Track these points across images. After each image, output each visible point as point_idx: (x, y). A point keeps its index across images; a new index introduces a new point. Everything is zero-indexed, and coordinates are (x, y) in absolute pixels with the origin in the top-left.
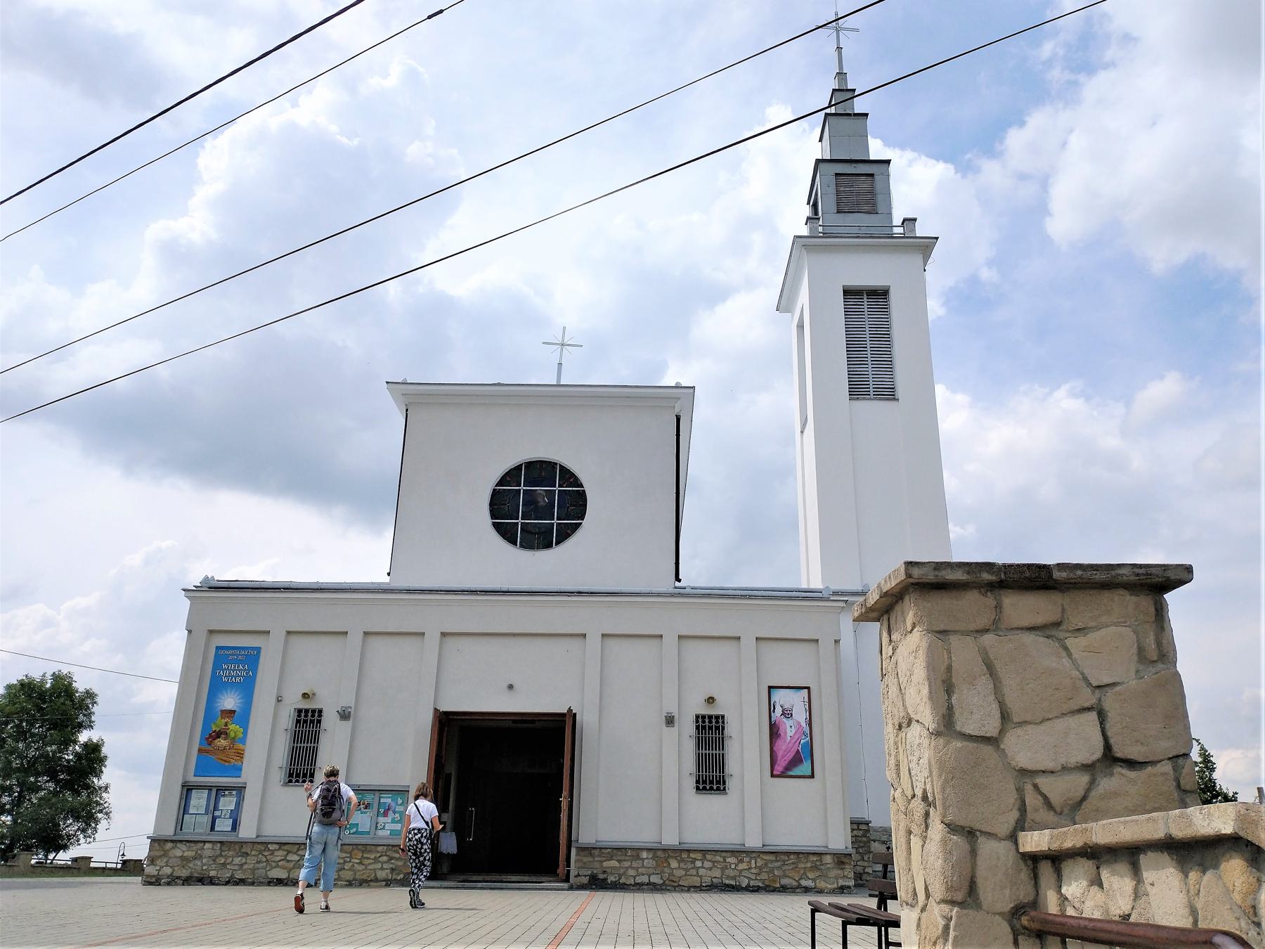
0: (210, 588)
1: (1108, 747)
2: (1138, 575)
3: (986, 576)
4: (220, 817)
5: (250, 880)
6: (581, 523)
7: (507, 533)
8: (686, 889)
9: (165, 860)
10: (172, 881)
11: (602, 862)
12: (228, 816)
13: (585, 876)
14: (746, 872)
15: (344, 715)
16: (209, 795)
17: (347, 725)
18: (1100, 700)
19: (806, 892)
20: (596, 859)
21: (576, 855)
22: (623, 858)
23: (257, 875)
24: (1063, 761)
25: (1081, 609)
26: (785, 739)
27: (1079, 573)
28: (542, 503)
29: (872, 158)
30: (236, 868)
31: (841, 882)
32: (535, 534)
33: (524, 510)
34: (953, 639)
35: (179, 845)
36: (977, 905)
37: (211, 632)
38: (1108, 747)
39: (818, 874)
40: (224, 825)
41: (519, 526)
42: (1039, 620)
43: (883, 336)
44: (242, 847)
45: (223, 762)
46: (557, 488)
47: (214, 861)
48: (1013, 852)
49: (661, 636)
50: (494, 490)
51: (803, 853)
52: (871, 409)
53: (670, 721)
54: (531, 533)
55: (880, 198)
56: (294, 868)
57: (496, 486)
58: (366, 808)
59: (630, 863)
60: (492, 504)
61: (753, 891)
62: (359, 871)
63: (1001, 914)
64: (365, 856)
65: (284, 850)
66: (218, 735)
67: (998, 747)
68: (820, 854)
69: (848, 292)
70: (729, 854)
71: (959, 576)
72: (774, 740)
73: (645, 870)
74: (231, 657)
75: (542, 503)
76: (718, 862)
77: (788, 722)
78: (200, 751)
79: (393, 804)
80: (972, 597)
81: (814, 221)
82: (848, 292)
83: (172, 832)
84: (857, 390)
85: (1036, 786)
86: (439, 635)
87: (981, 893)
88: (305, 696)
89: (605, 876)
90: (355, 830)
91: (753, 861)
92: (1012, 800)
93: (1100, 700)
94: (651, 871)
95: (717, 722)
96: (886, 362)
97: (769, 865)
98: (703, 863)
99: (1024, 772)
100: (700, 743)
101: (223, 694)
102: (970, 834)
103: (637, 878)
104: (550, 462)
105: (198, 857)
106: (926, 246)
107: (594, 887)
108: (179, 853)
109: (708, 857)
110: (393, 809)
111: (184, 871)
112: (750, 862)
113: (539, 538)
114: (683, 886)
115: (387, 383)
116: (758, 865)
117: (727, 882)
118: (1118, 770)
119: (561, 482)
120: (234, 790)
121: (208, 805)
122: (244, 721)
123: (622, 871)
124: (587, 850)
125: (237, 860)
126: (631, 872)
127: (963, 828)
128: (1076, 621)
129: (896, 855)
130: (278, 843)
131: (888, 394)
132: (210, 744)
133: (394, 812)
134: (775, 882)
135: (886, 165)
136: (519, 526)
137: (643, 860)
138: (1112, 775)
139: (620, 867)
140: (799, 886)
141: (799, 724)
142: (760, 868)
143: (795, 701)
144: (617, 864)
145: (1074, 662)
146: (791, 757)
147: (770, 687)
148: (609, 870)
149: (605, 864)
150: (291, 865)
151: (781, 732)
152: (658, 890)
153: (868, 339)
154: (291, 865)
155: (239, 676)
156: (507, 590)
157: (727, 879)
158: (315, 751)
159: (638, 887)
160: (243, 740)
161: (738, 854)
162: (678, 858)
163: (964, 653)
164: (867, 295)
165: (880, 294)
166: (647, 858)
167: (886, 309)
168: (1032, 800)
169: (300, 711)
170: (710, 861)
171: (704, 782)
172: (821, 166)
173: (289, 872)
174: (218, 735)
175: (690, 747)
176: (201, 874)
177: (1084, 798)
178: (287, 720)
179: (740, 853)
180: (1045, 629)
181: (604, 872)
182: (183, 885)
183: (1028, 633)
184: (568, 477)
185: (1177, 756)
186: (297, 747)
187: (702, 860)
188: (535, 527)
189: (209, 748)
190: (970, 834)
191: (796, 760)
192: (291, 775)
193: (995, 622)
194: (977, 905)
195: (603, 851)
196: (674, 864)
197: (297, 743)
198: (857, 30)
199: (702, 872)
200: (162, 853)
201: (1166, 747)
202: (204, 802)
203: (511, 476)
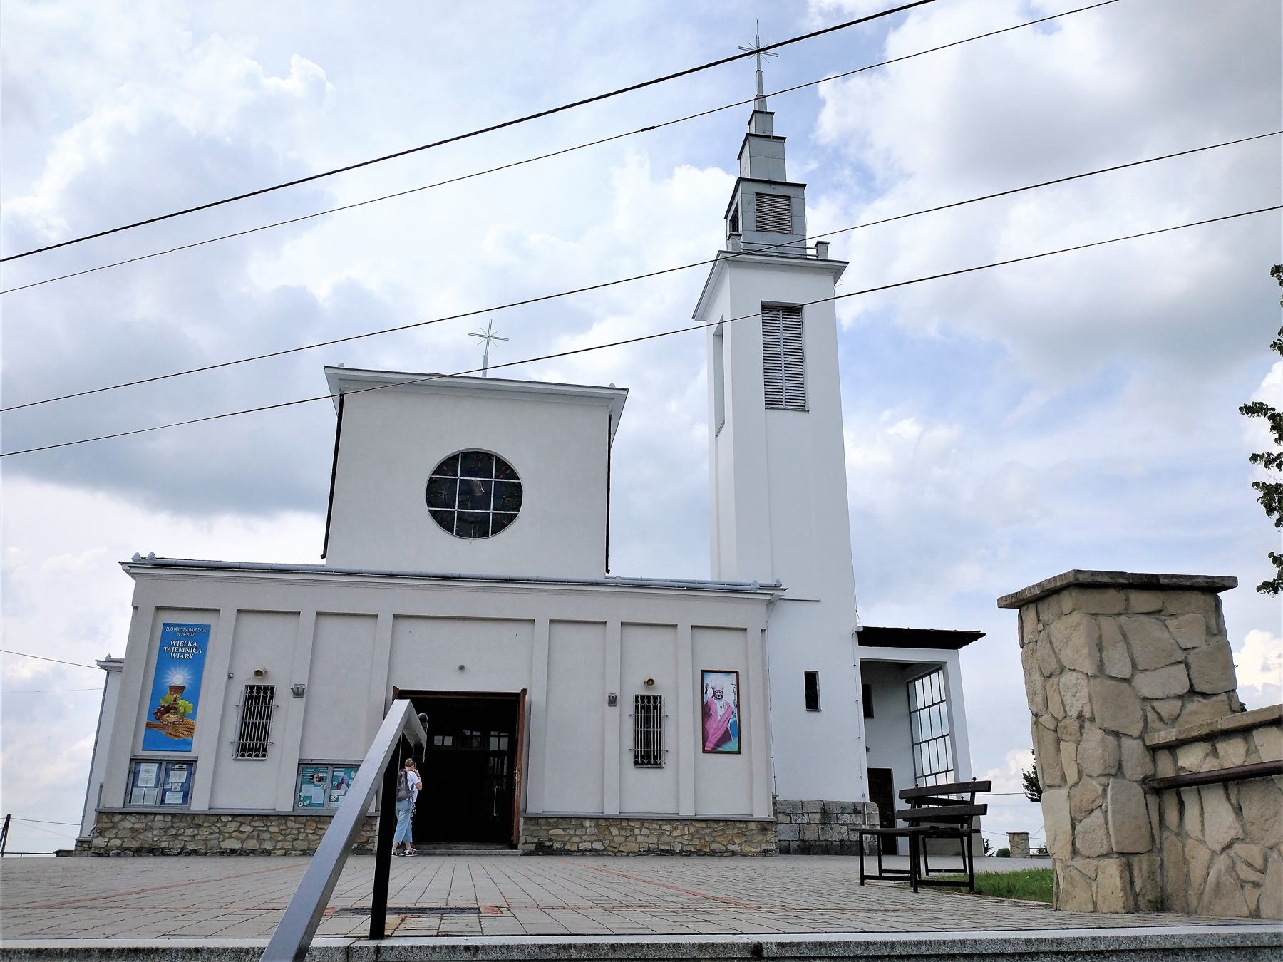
0: (154, 565)
1: (1191, 685)
2: (1208, 582)
3: (1121, 581)
4: (170, 790)
5: (203, 851)
6: (517, 514)
7: (444, 522)
8: (626, 854)
9: (114, 832)
10: (122, 852)
11: (548, 830)
12: (178, 789)
13: (533, 843)
14: (680, 838)
15: (298, 693)
16: (159, 769)
17: (300, 702)
18: (1186, 657)
19: (733, 856)
20: (543, 828)
21: (524, 824)
22: (567, 827)
23: (209, 846)
24: (1167, 692)
25: (1174, 602)
26: (716, 718)
27: (1174, 580)
28: (478, 494)
29: (788, 181)
30: (188, 839)
31: (764, 847)
32: (472, 523)
34: (1100, 618)
35: (128, 817)
36: (1124, 777)
37: (158, 608)
38: (1191, 685)
39: (743, 839)
40: (174, 798)
41: (456, 515)
42: (1151, 609)
43: (797, 351)
44: (193, 819)
45: (173, 737)
46: (493, 479)
47: (164, 832)
48: (1141, 746)
49: (605, 623)
50: (431, 478)
51: (731, 821)
52: (785, 419)
53: (613, 701)
54: (466, 521)
56: (247, 838)
57: (432, 474)
58: (319, 781)
59: (574, 831)
60: (428, 492)
61: (686, 855)
62: (313, 841)
63: (1137, 781)
64: (319, 826)
65: (237, 822)
66: (168, 710)
67: (1130, 685)
68: (746, 822)
70: (665, 823)
71: (1106, 580)
72: (706, 719)
73: (588, 837)
74: (179, 634)
75: (478, 494)
76: (654, 829)
77: (718, 703)
79: (346, 777)
80: (1111, 593)
81: (736, 237)
84: (772, 400)
85: (1153, 708)
86: (392, 616)
87: (1125, 769)
88: (258, 673)
89: (551, 843)
90: (308, 802)
91: (686, 829)
92: (1140, 716)
93: (1186, 657)
94: (594, 838)
95: (655, 702)
96: (799, 376)
97: (701, 832)
98: (641, 831)
99: (1145, 699)
100: (640, 722)
101: (167, 674)
102: (1117, 734)
103: (581, 844)
104: (487, 454)
105: (148, 829)
106: (837, 269)
107: (540, 853)
108: (128, 825)
109: (646, 825)
110: (346, 782)
111: (135, 842)
112: (683, 829)
113: (475, 527)
114: (623, 852)
115: (325, 367)
116: (691, 832)
117: (663, 847)
118: (1197, 698)
119: (497, 474)
120: (185, 764)
122: (194, 697)
123: (567, 838)
124: (534, 820)
125: (189, 832)
126: (576, 840)
127: (1113, 731)
128: (1171, 609)
130: (230, 815)
131: (800, 405)
132: (158, 719)
134: (705, 846)
135: (802, 189)
136: (456, 515)
137: (586, 828)
138: (1193, 702)
139: (565, 835)
140: (727, 851)
141: (728, 704)
142: (693, 835)
143: (724, 684)
144: (562, 833)
145: (1171, 633)
146: (721, 735)
147: (703, 672)
148: (554, 838)
149: (551, 832)
150: (244, 836)
151: (712, 712)
152: (599, 855)
153: (782, 353)
154: (246, 835)
155: (187, 652)
156: (458, 576)
157: (662, 844)
158: (267, 726)
159: (583, 852)
160: (193, 715)
161: (672, 822)
162: (619, 826)
163: (1109, 627)
164: (783, 312)
165: (795, 310)
166: (590, 827)
167: (799, 326)
168: (1151, 716)
169: (252, 688)
170: (647, 828)
171: (643, 757)
172: (743, 184)
173: (242, 842)
174: (168, 710)
175: (630, 726)
176: (151, 845)
177: (1179, 715)
178: (238, 697)
179: (673, 821)
181: (550, 840)
182: (133, 856)
183: (1144, 616)
184: (505, 469)
185: (1229, 691)
186: (249, 723)
187: (642, 827)
188: (472, 516)
190: (1117, 734)
191: (726, 738)
192: (244, 750)
193: (1126, 609)
194: (1124, 777)
195: (549, 820)
196: (615, 832)
197: (250, 718)
199: (640, 838)
200: (111, 825)
201: (1223, 685)
202: (154, 776)
203: (448, 465)
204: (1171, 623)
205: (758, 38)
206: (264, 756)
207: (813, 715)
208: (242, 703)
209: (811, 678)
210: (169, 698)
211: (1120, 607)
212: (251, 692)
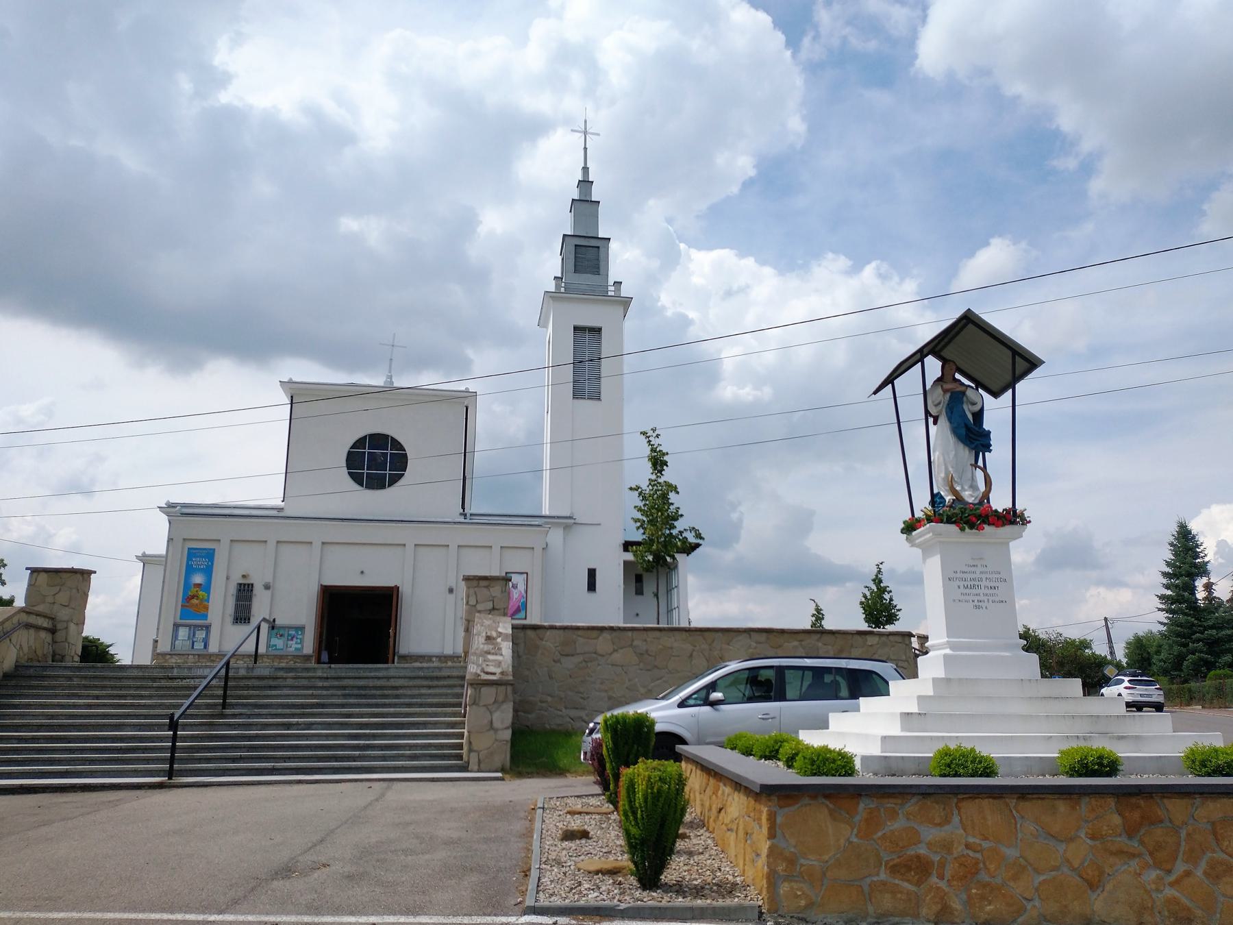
0: (182, 514)
7: (357, 479)
15: (267, 587)
17: (269, 593)
28: (380, 461)
29: (599, 237)
35: (174, 656)
40: (199, 646)
50: (349, 451)
55: (602, 264)
60: (347, 460)
66: (193, 597)
69: (576, 329)
78: (182, 606)
82: (576, 329)
83: (169, 650)
84: (578, 394)
88: (244, 576)
121: (189, 634)
133: (297, 638)
141: (521, 592)
158: (250, 605)
163: (472, 591)
169: (240, 584)
172: (566, 238)
174: (193, 597)
178: (233, 590)
180: (487, 587)
184: (397, 444)
189: (187, 604)
192: (237, 619)
198: (598, 135)
203: (360, 443)
204: (491, 589)
205: (586, 122)
206: (249, 622)
207: (592, 595)
208: (235, 592)
209: (592, 573)
210: (193, 591)
211: (476, 585)
212: (240, 587)
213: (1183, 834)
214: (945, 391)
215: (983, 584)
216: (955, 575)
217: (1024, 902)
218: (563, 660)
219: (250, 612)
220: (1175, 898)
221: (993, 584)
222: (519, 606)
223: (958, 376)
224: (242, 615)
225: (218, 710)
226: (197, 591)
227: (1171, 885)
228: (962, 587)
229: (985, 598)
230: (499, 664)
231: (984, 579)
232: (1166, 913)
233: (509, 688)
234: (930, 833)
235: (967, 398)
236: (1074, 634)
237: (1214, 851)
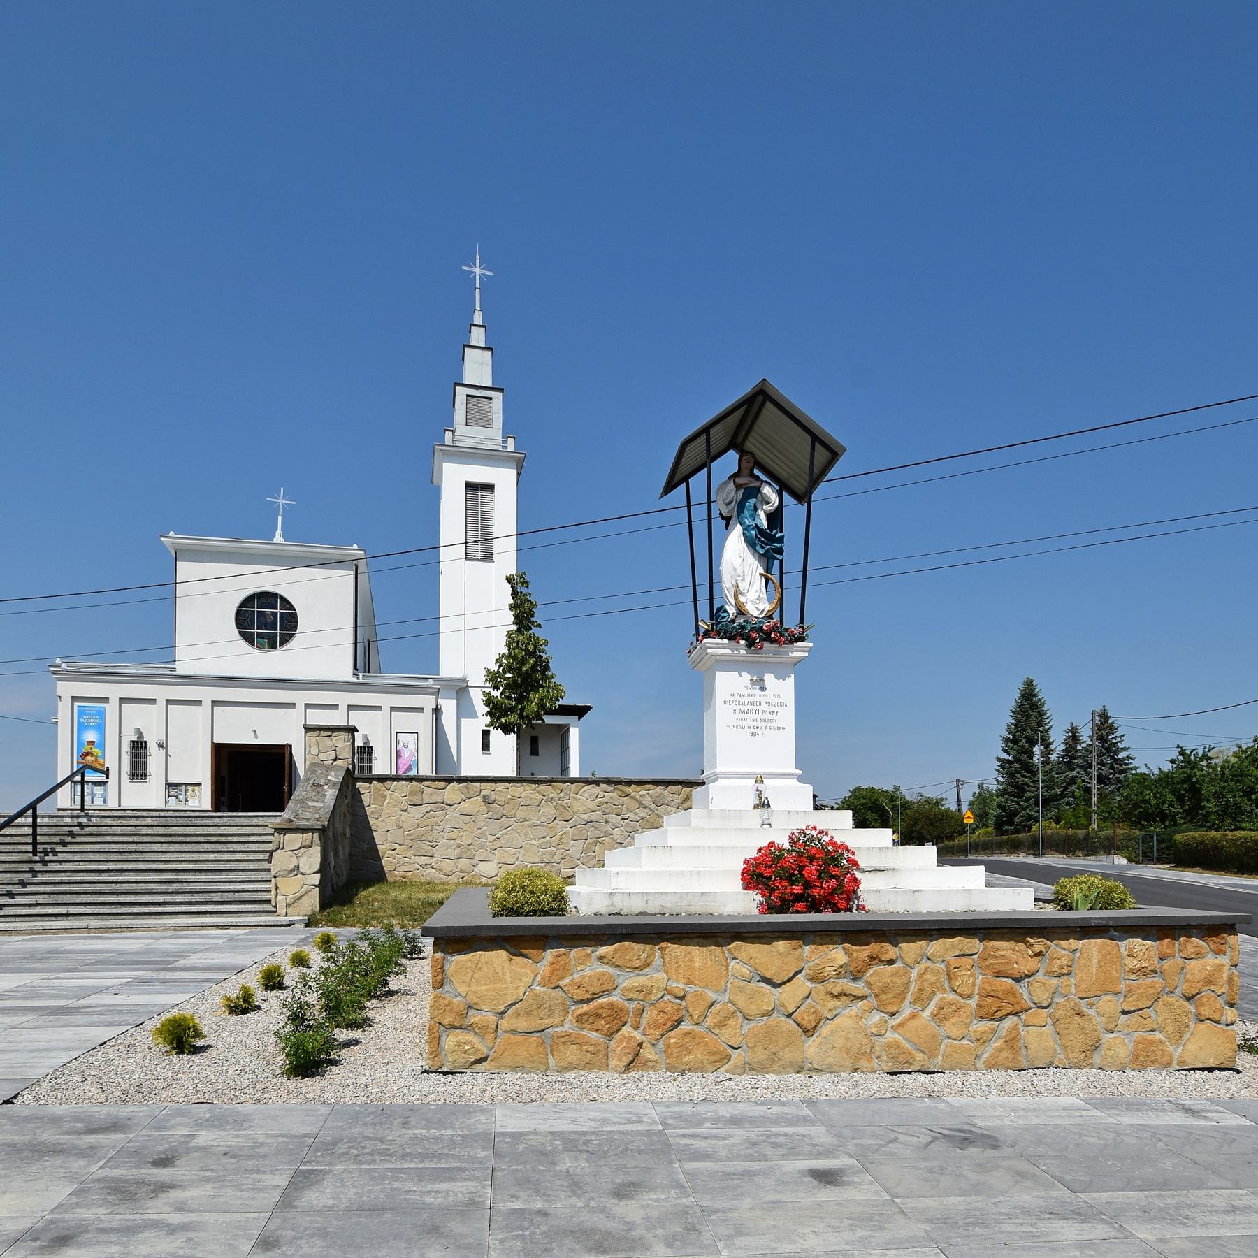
33: (271, 635)
46: (278, 610)
60: (237, 619)
66: (87, 754)
77: (406, 750)
122: (102, 746)
129: (315, 900)
132: (83, 759)
147: (397, 733)
174: (87, 754)
184: (286, 603)
192: (133, 775)
203: (248, 601)
210: (87, 748)
212: (134, 744)
213: (914, 973)
214: (738, 487)
215: (761, 708)
216: (732, 698)
217: (730, 1050)
218: (411, 809)
219: (145, 769)
220: (896, 1042)
221: (772, 709)
222: (410, 765)
223: (756, 472)
224: (139, 773)
225: (24, 857)
226: (91, 749)
227: (894, 1028)
228: (738, 711)
229: (763, 724)
230: (317, 810)
231: (763, 703)
232: (885, 1058)
233: (316, 835)
234: (628, 981)
235: (762, 496)
236: (932, 794)
237: (944, 991)
